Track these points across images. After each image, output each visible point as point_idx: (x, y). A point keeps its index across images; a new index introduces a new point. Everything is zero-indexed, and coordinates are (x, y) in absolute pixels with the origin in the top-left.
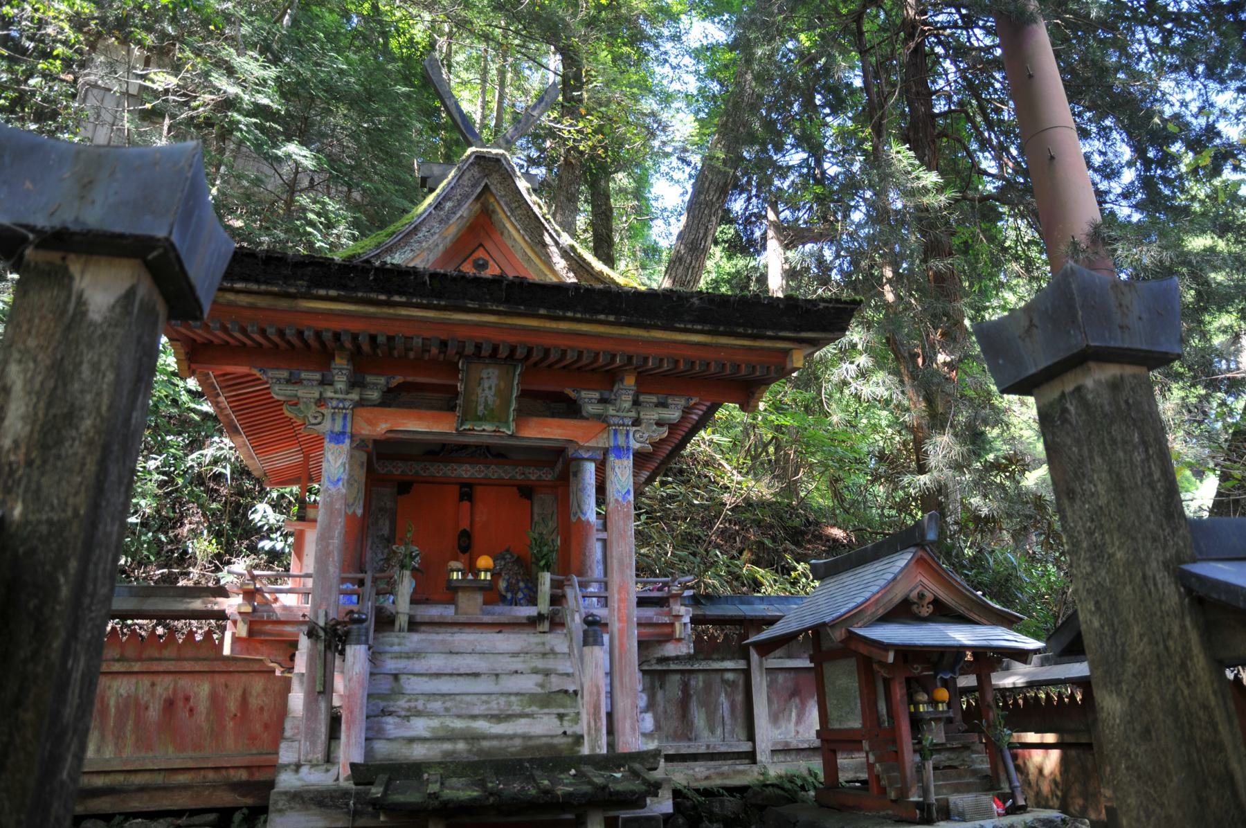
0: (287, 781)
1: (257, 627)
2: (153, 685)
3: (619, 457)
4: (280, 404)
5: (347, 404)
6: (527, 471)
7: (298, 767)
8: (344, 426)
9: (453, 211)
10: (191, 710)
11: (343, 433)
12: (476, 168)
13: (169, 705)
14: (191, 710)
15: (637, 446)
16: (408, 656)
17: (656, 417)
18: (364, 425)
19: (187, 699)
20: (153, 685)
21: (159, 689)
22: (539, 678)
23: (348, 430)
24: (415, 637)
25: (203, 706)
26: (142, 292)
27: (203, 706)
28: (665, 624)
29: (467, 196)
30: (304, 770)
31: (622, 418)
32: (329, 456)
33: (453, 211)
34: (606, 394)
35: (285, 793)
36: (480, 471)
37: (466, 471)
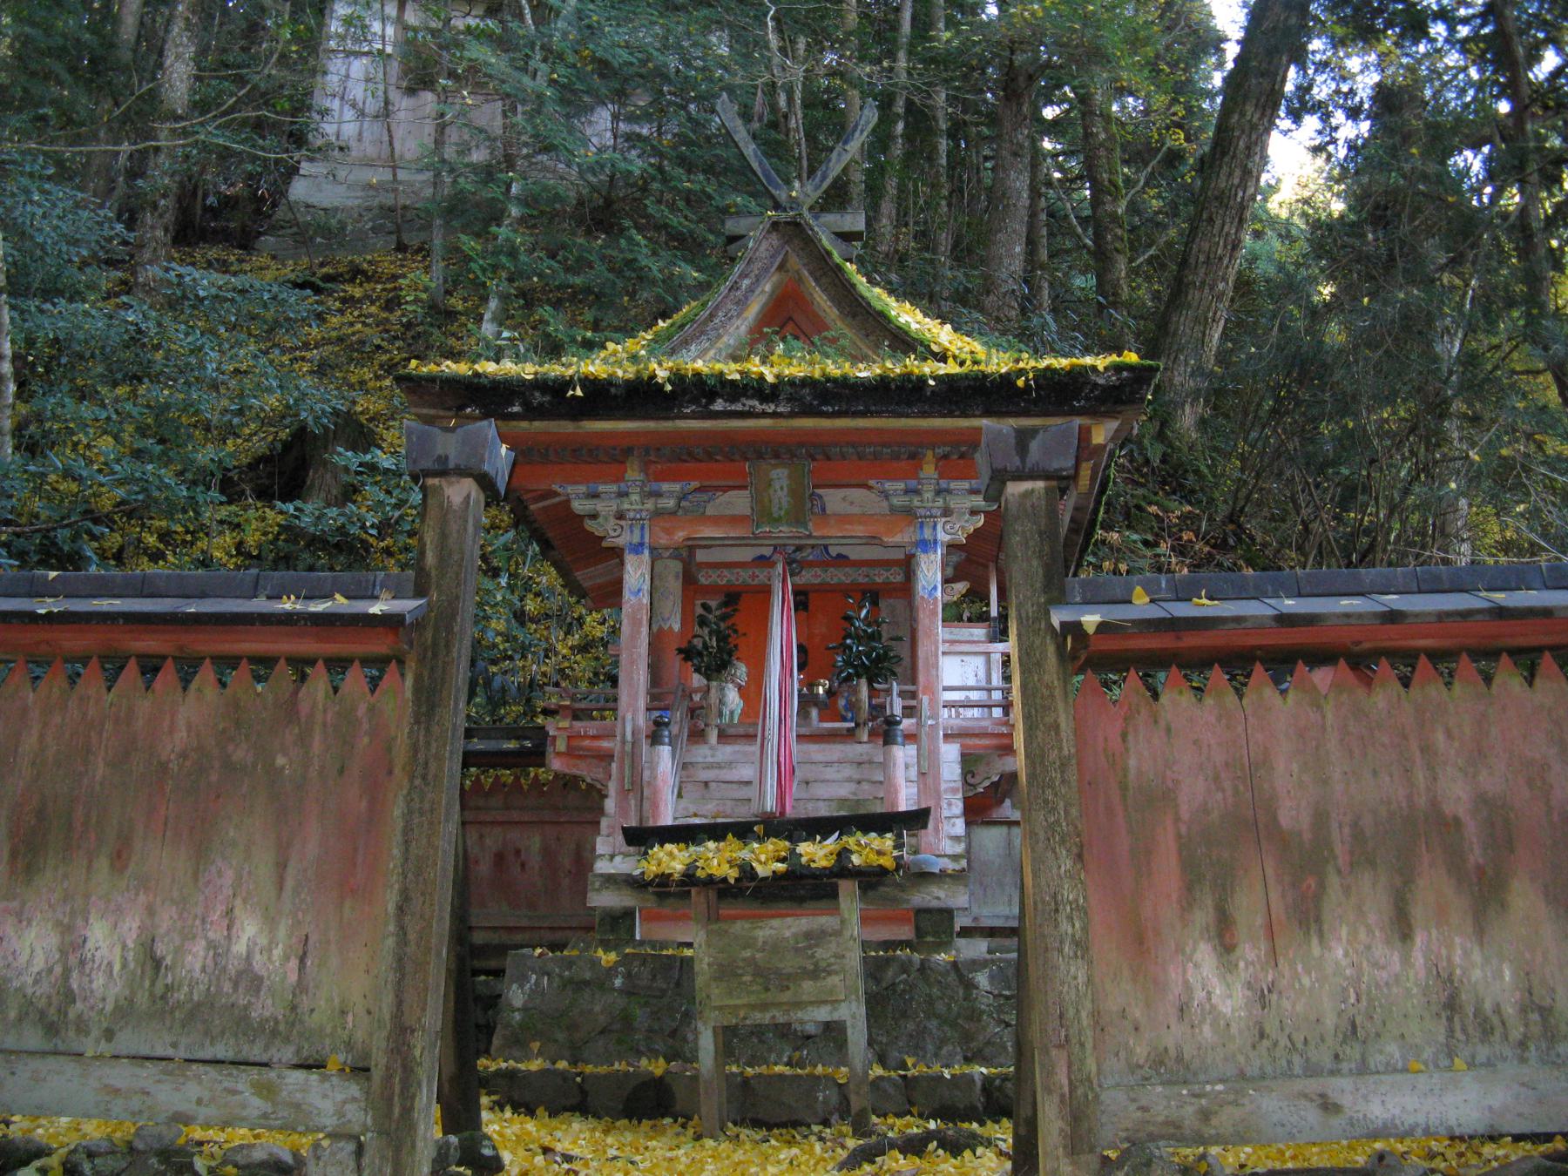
0: (602, 867)
1: (575, 743)
2: (481, 836)
3: (925, 552)
4: (581, 517)
5: (644, 514)
6: (872, 572)
7: (612, 857)
8: (642, 536)
9: (751, 290)
10: (523, 865)
11: (641, 544)
12: (774, 236)
13: (499, 858)
14: (523, 865)
15: (947, 538)
16: (719, 766)
17: (968, 505)
18: (662, 534)
19: (518, 852)
20: (481, 836)
21: (488, 841)
22: (853, 786)
23: (647, 540)
24: (728, 749)
25: (535, 861)
26: (473, 495)
27: (535, 861)
28: (1002, 735)
29: (766, 270)
30: (618, 859)
31: (930, 509)
32: (629, 567)
33: (751, 290)
34: (913, 483)
35: (602, 875)
36: (816, 576)
37: (816, 576)
